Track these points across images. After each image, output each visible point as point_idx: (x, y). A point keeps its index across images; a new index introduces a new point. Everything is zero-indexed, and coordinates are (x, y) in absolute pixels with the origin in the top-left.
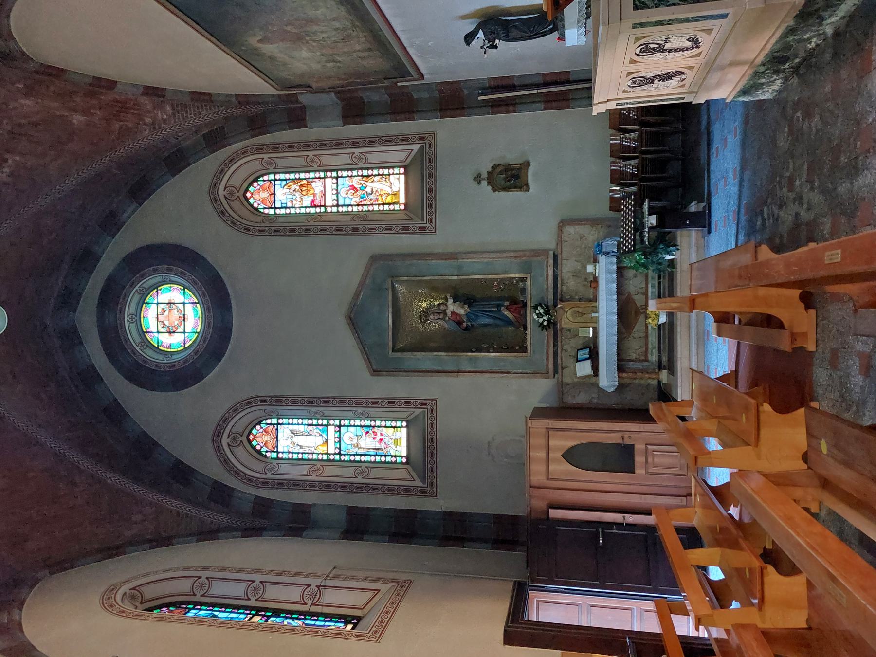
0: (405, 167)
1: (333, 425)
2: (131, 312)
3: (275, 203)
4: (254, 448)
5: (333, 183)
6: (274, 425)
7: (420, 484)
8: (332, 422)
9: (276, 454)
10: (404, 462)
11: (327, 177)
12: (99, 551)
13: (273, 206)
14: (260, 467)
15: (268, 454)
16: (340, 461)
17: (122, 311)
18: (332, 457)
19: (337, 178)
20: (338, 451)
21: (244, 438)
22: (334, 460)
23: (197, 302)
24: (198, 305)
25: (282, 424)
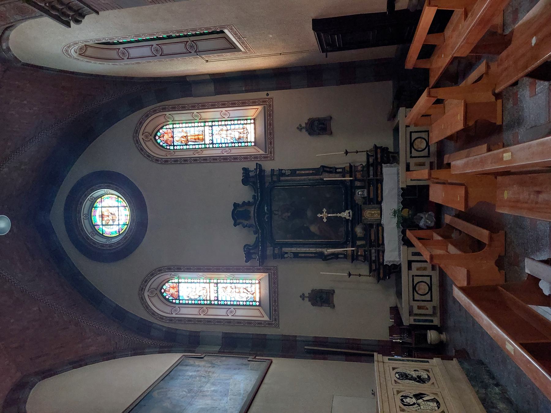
0: (254, 119)
1: (213, 283)
2: (85, 213)
3: (173, 143)
4: (165, 297)
5: (214, 286)
6: (170, 129)
7: (263, 153)
8: (212, 281)
9: (178, 301)
10: (258, 305)
11: (206, 126)
12: (70, 364)
13: (172, 145)
14: (163, 153)
15: (174, 301)
16: (218, 304)
17: (80, 212)
18: (208, 146)
19: (212, 126)
20: (212, 142)
21: (159, 291)
22: (214, 304)
23: (126, 205)
24: (127, 208)
25: (176, 128)
